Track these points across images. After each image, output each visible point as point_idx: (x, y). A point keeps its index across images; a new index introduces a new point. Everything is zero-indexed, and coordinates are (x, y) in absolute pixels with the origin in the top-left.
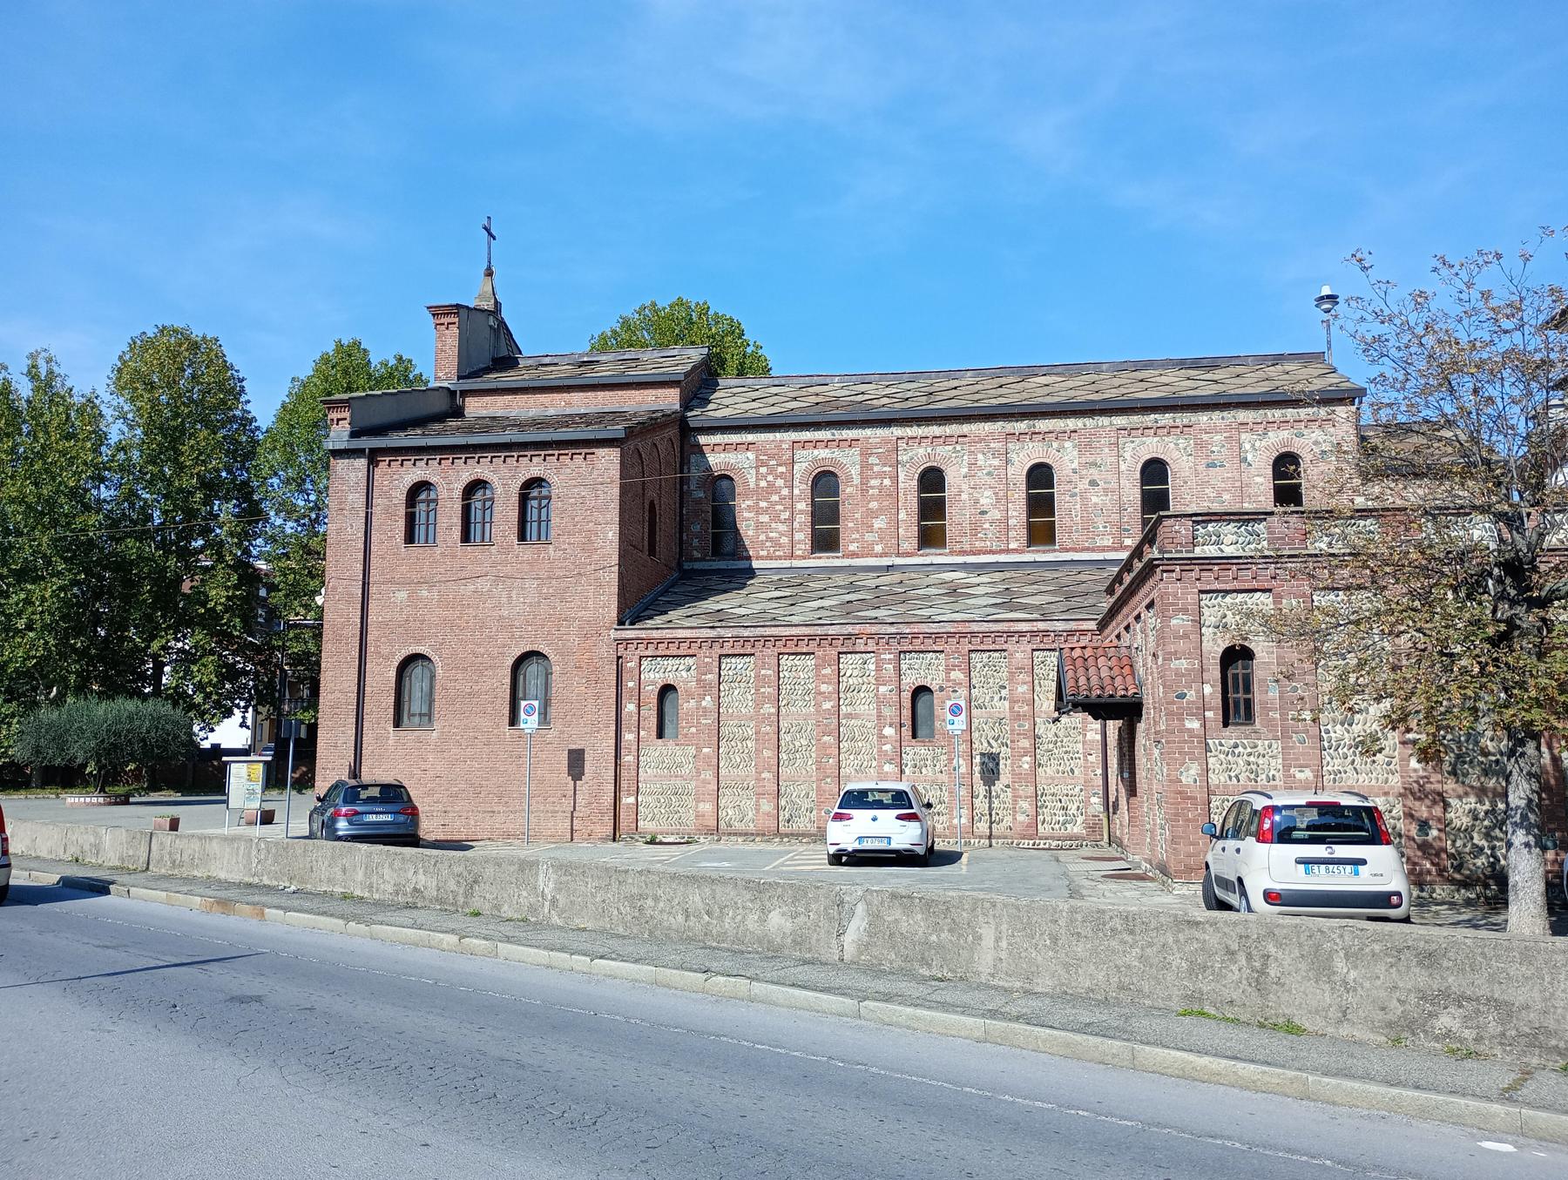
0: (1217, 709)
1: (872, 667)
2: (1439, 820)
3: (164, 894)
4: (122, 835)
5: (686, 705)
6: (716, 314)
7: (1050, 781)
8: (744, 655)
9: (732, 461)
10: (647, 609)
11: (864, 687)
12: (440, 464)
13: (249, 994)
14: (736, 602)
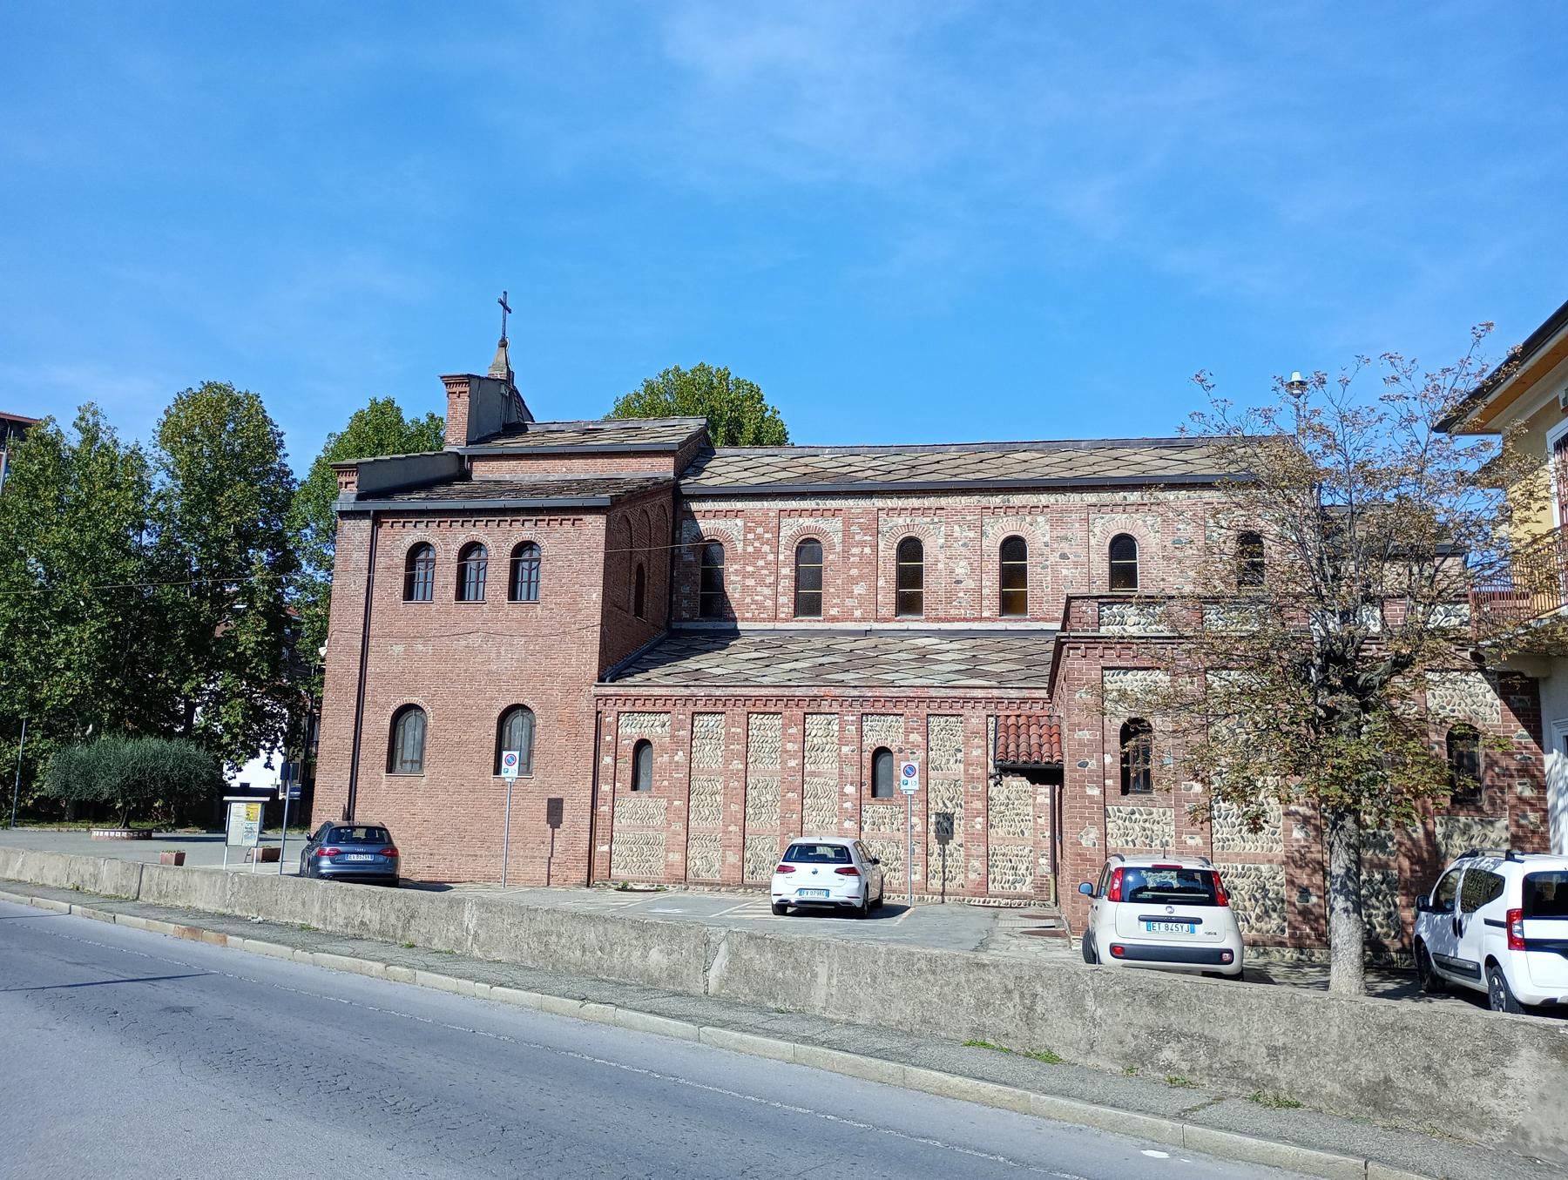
0: (1116, 777)
1: (836, 728)
2: (1319, 888)
3: (144, 921)
4: (118, 866)
5: (660, 760)
6: (737, 379)
7: (1001, 842)
8: (716, 713)
9: (722, 527)
10: (630, 666)
11: (828, 747)
12: (439, 526)
13: (183, 1005)
14: (714, 663)
